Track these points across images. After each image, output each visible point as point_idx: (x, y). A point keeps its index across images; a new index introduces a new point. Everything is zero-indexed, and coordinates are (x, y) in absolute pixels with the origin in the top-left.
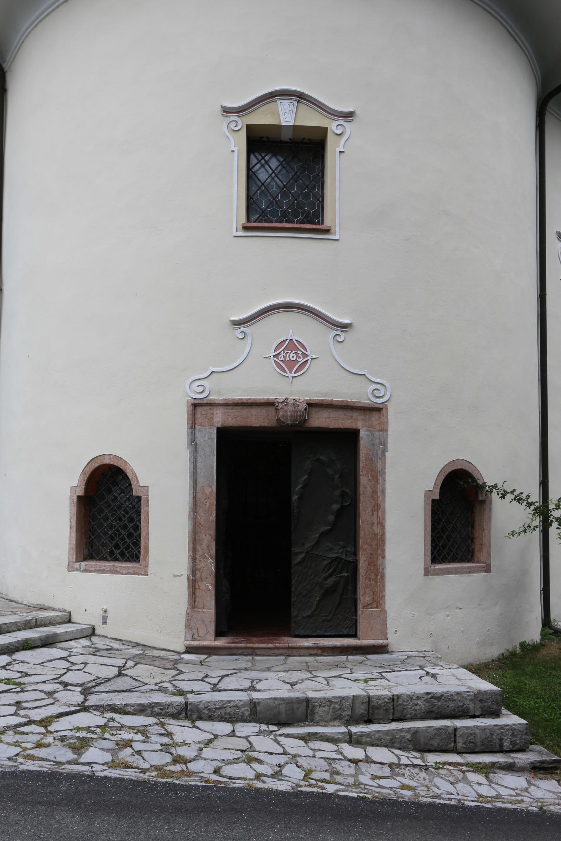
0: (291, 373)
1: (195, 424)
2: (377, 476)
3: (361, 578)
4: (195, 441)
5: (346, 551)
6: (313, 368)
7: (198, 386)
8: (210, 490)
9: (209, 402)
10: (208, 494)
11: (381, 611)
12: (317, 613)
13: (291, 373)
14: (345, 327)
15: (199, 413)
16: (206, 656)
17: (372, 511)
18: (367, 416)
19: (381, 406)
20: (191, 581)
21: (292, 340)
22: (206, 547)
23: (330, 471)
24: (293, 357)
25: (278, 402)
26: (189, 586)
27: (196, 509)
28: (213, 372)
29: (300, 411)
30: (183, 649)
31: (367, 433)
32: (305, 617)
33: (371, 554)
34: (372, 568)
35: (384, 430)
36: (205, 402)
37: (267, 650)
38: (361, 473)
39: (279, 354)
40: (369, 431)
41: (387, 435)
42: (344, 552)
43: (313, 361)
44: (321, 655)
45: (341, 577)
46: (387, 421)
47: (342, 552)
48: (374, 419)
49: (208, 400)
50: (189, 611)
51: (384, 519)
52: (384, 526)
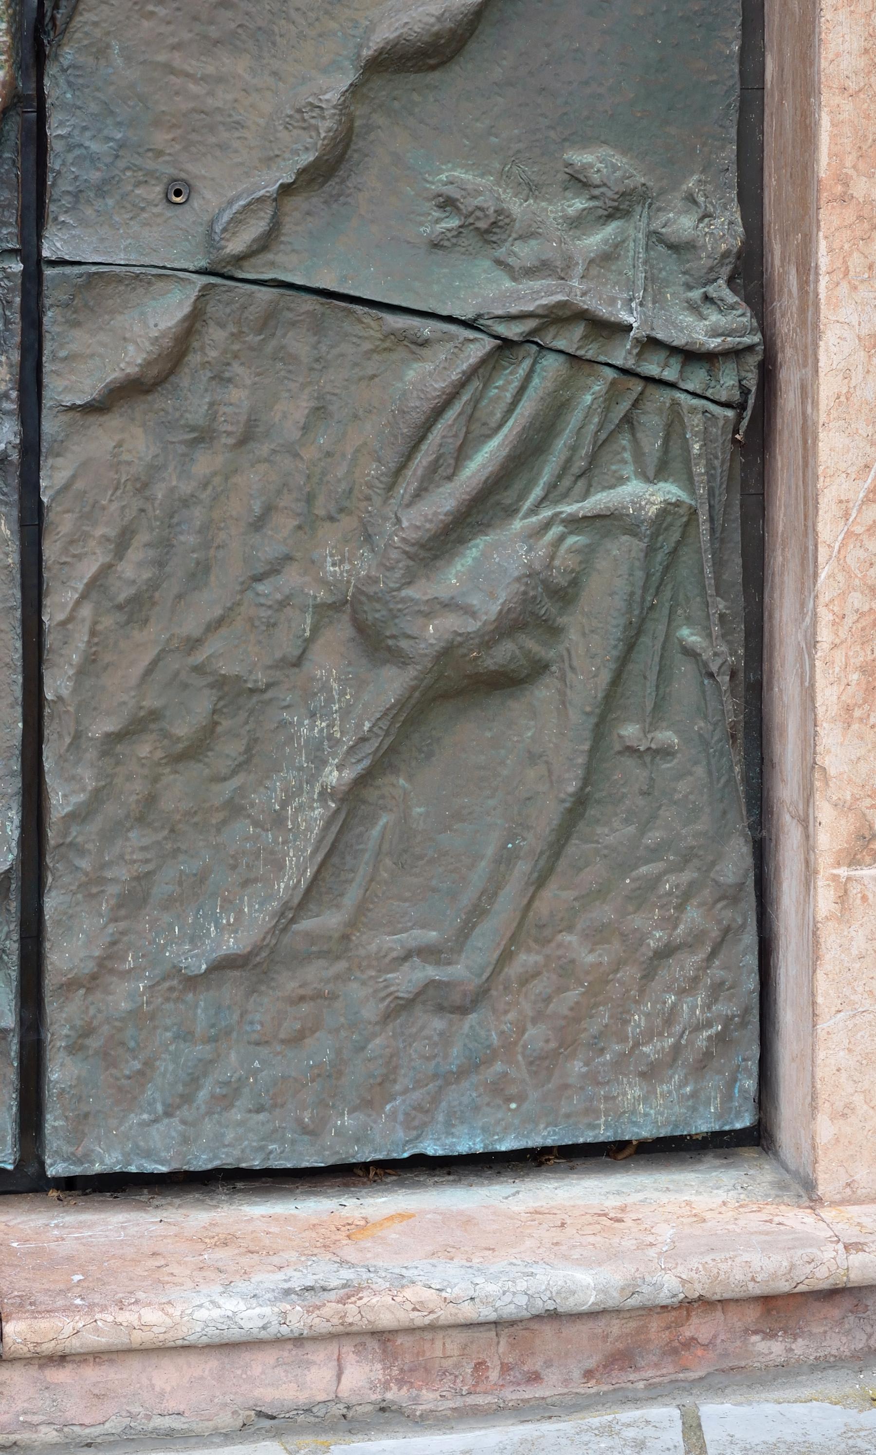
12: (327, 921)
32: (192, 982)
42: (635, 248)
47: (607, 257)
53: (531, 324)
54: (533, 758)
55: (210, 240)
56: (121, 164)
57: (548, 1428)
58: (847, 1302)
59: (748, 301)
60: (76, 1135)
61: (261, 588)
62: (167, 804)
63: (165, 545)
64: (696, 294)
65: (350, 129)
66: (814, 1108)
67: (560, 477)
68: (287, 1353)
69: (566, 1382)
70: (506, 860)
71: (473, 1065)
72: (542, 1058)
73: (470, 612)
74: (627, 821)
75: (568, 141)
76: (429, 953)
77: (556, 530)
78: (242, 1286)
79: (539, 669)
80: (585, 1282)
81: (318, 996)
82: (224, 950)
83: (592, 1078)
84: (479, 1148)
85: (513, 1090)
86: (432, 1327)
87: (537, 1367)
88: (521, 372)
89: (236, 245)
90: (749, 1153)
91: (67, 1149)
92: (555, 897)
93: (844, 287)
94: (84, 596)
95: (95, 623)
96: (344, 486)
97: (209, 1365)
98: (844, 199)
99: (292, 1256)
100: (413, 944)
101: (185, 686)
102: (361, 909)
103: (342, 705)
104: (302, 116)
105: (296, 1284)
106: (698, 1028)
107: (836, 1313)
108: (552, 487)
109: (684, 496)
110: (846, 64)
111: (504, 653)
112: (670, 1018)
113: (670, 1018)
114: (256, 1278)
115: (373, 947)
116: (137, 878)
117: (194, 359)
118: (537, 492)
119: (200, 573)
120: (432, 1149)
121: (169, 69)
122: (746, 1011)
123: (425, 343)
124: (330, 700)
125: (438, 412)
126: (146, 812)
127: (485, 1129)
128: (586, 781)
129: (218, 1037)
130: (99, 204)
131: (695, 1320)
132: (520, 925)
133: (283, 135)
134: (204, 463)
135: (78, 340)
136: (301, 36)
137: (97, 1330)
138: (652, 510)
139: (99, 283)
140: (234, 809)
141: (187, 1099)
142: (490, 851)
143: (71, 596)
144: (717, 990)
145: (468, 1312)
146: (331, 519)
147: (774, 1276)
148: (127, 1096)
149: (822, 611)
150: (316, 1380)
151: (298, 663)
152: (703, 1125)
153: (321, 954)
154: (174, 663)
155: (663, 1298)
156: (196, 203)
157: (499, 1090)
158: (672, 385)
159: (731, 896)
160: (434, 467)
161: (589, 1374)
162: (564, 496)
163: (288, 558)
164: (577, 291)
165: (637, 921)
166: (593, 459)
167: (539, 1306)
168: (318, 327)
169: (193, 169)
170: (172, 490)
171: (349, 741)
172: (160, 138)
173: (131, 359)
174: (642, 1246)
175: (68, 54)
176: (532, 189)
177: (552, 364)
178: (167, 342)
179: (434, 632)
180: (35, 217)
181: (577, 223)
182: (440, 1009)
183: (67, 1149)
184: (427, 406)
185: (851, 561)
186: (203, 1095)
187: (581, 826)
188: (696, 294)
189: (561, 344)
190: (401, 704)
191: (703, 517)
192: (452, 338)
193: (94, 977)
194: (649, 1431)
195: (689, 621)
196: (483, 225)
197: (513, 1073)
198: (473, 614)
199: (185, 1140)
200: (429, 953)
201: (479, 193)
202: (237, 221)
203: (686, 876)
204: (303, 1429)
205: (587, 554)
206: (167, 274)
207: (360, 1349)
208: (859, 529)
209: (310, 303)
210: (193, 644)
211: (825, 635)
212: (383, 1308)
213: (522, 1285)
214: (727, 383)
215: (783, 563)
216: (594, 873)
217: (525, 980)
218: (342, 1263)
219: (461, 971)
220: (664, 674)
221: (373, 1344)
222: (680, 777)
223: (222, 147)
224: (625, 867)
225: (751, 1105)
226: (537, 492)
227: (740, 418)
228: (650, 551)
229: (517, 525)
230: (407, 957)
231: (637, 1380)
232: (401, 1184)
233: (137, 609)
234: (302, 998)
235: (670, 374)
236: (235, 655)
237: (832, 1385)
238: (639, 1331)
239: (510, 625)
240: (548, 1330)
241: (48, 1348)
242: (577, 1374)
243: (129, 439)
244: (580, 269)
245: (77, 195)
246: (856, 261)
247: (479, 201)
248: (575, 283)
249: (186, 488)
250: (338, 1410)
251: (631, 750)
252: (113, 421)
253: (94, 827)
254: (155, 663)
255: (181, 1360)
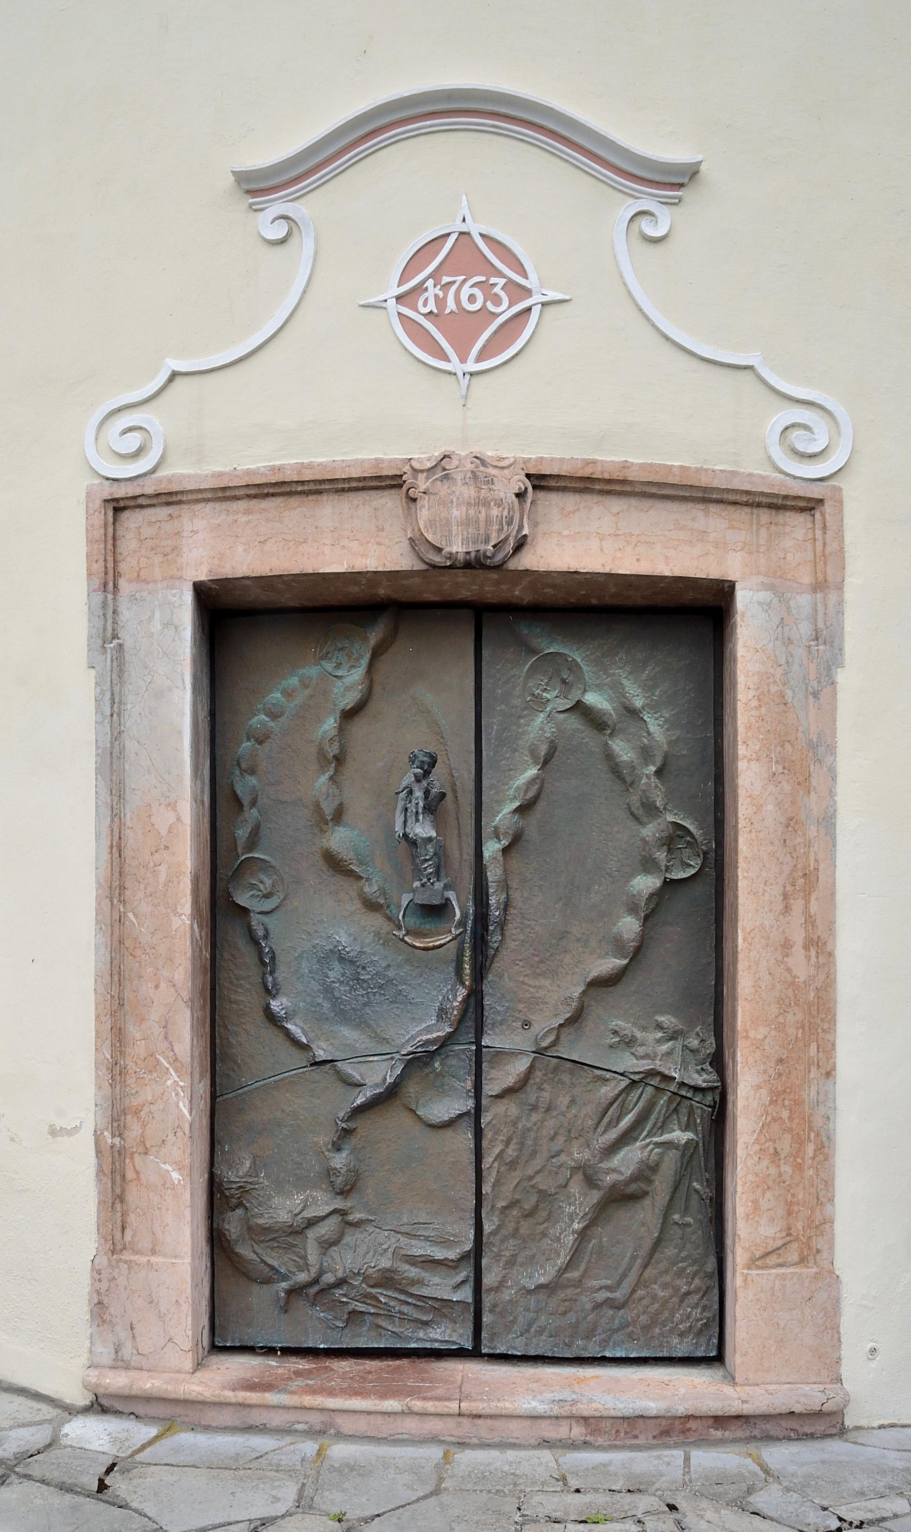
0: (463, 360)
1: (117, 575)
2: (807, 762)
3: (741, 1152)
4: (115, 636)
5: (685, 1047)
6: (550, 342)
7: (124, 432)
8: (170, 817)
9: (164, 488)
10: (164, 833)
11: (816, 1277)
12: (575, 1274)
13: (463, 360)
14: (676, 180)
15: (130, 535)
16: (152, 1431)
17: (785, 896)
18: (763, 532)
19: (815, 492)
20: (107, 1153)
21: (468, 234)
22: (157, 1031)
23: (623, 750)
24: (472, 298)
25: (415, 471)
26: (100, 1171)
27: (122, 888)
28: (174, 375)
29: (499, 503)
30: (82, 1399)
31: (764, 596)
32: (530, 1292)
33: (781, 1061)
34: (785, 1114)
35: (826, 583)
36: (149, 490)
37: (379, 1419)
38: (742, 750)
39: (420, 288)
40: (771, 588)
41: (841, 603)
42: (678, 1051)
43: (551, 311)
44: (586, 1445)
45: (668, 1145)
46: (842, 549)
47: (669, 1053)
48: (788, 543)
49: (160, 481)
50: (103, 1261)
51: (831, 926)
52: (831, 955)
53: (642, 1075)
54: (643, 1224)
55: (536, 1042)
56: (508, 1014)
57: (639, 1454)
58: (744, 1420)
59: (717, 1072)
60: (491, 1340)
61: (553, 1160)
62: (522, 1231)
63: (522, 1144)
64: (699, 1068)
65: (583, 1006)
66: (735, 1352)
67: (653, 1128)
68: (553, 1421)
69: (647, 1439)
70: (634, 1258)
71: (622, 1327)
72: (646, 1327)
73: (621, 1173)
74: (675, 1248)
75: (656, 1013)
76: (608, 1288)
77: (651, 1146)
78: (539, 1397)
79: (646, 1193)
80: (652, 1406)
81: (571, 1300)
82: (540, 1282)
83: (662, 1334)
84: (624, 1356)
85: (635, 1337)
86: (601, 1417)
87: (637, 1433)
88: (639, 1092)
89: (544, 1044)
90: (717, 1364)
91: (488, 1344)
92: (649, 1272)
93: (746, 1069)
94: (495, 1160)
95: (499, 1169)
96: (580, 1127)
97: (528, 1423)
98: (747, 1037)
99: (558, 1388)
100: (603, 1285)
101: (528, 1192)
102: (585, 1271)
103: (578, 1203)
104: (567, 1000)
105: (557, 1399)
106: (698, 1320)
107: (740, 1423)
108: (650, 1132)
109: (695, 1137)
110: (747, 990)
111: (632, 1188)
112: (688, 1317)
113: (689, 1316)
114: (544, 1395)
115: (589, 1285)
116: (512, 1256)
117: (531, 1081)
118: (645, 1133)
119: (533, 1154)
120: (608, 1354)
121: (523, 983)
122: (714, 1316)
123: (607, 1080)
124: (576, 1200)
125: (611, 1104)
126: (515, 1234)
127: (626, 1349)
128: (661, 1233)
129: (538, 1311)
130: (500, 1028)
131: (691, 1422)
132: (638, 1281)
133: (560, 1007)
134: (535, 1117)
135: (494, 1073)
136: (567, 974)
137: (490, 1408)
138: (683, 1142)
139: (501, 1055)
140: (544, 1235)
141: (528, 1331)
142: (628, 1255)
143: (491, 1159)
144: (704, 1308)
145: (613, 1413)
146: (576, 1138)
147: (717, 1410)
148: (508, 1328)
149: (738, 1180)
150: (562, 1431)
151: (565, 1187)
152: (699, 1354)
153: (572, 1286)
154: (525, 1184)
155: (679, 1414)
156: (532, 1029)
157: (630, 1336)
158: (691, 1099)
159: (710, 1276)
160: (610, 1122)
161: (654, 1437)
162: (654, 1135)
163: (562, 1151)
164: (658, 1065)
165: (678, 1282)
166: (664, 1123)
167: (637, 1414)
168: (572, 1073)
169: (532, 1017)
170: (524, 1125)
171: (581, 1214)
172: (521, 1006)
173: (510, 1081)
174: (674, 1395)
175: (490, 977)
176: (644, 1029)
177: (649, 1089)
178: (522, 1075)
179: (609, 1179)
180: (479, 1032)
181: (659, 1041)
182: (612, 1307)
183: (488, 1344)
184: (607, 1102)
185: (749, 1164)
186: (533, 1330)
187: (659, 1248)
188: (699, 1068)
189: (652, 1083)
190: (598, 1203)
191: (701, 1145)
192: (615, 1078)
193: (497, 1287)
194: (672, 1459)
195: (697, 1181)
196: (627, 1040)
197: (635, 1330)
198: (622, 1174)
199: (527, 1345)
200: (608, 1288)
201: (625, 1030)
202: (545, 1035)
203: (695, 1268)
204: (558, 1447)
205: (662, 1155)
206: (522, 1053)
207: (578, 1422)
208: (751, 1153)
209: (569, 1065)
210: (531, 1178)
211: (739, 1189)
212: (585, 1409)
213: (631, 1405)
214: (709, 1099)
215: (728, 1161)
216: (663, 1266)
217: (640, 1300)
218: (574, 1392)
219: (617, 1295)
220: (688, 1199)
221: (582, 1421)
222: (693, 1233)
223: (541, 1010)
224: (674, 1264)
225: (715, 1348)
226: (645, 1133)
227: (713, 1111)
228: (683, 1156)
229: (638, 1144)
230: (601, 1288)
231: (671, 1441)
232: (599, 1365)
233: (513, 1165)
234: (566, 1300)
235: (689, 1095)
236: (544, 1182)
237: (736, 1448)
238: (671, 1424)
239: (635, 1178)
240: (640, 1421)
241: (474, 1412)
242: (650, 1437)
243: (510, 1108)
244: (659, 1057)
245: (493, 1024)
246: (751, 1059)
247: (625, 1032)
248: (657, 1062)
249: (529, 1125)
250: (570, 1442)
251: (677, 1223)
252: (505, 1101)
253: (498, 1237)
254: (518, 1183)
255: (518, 1420)
